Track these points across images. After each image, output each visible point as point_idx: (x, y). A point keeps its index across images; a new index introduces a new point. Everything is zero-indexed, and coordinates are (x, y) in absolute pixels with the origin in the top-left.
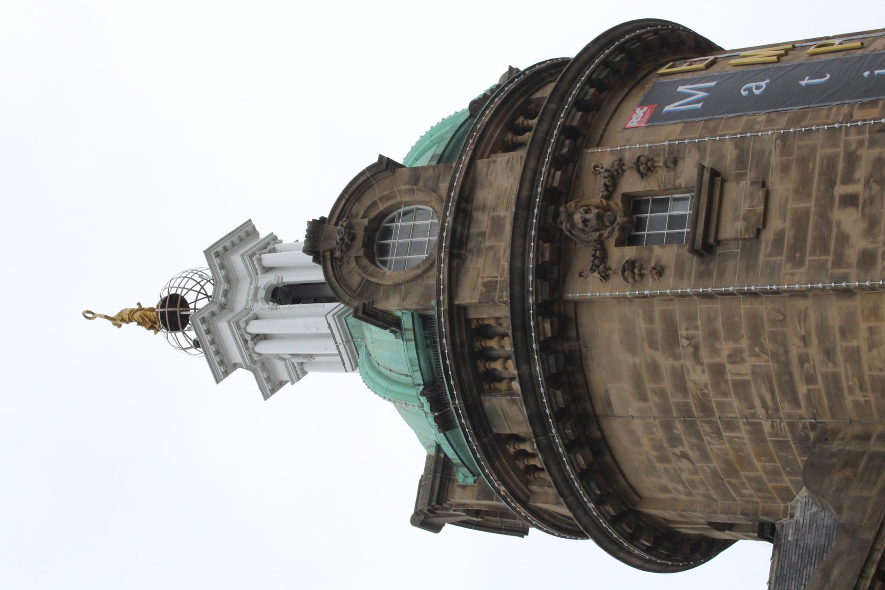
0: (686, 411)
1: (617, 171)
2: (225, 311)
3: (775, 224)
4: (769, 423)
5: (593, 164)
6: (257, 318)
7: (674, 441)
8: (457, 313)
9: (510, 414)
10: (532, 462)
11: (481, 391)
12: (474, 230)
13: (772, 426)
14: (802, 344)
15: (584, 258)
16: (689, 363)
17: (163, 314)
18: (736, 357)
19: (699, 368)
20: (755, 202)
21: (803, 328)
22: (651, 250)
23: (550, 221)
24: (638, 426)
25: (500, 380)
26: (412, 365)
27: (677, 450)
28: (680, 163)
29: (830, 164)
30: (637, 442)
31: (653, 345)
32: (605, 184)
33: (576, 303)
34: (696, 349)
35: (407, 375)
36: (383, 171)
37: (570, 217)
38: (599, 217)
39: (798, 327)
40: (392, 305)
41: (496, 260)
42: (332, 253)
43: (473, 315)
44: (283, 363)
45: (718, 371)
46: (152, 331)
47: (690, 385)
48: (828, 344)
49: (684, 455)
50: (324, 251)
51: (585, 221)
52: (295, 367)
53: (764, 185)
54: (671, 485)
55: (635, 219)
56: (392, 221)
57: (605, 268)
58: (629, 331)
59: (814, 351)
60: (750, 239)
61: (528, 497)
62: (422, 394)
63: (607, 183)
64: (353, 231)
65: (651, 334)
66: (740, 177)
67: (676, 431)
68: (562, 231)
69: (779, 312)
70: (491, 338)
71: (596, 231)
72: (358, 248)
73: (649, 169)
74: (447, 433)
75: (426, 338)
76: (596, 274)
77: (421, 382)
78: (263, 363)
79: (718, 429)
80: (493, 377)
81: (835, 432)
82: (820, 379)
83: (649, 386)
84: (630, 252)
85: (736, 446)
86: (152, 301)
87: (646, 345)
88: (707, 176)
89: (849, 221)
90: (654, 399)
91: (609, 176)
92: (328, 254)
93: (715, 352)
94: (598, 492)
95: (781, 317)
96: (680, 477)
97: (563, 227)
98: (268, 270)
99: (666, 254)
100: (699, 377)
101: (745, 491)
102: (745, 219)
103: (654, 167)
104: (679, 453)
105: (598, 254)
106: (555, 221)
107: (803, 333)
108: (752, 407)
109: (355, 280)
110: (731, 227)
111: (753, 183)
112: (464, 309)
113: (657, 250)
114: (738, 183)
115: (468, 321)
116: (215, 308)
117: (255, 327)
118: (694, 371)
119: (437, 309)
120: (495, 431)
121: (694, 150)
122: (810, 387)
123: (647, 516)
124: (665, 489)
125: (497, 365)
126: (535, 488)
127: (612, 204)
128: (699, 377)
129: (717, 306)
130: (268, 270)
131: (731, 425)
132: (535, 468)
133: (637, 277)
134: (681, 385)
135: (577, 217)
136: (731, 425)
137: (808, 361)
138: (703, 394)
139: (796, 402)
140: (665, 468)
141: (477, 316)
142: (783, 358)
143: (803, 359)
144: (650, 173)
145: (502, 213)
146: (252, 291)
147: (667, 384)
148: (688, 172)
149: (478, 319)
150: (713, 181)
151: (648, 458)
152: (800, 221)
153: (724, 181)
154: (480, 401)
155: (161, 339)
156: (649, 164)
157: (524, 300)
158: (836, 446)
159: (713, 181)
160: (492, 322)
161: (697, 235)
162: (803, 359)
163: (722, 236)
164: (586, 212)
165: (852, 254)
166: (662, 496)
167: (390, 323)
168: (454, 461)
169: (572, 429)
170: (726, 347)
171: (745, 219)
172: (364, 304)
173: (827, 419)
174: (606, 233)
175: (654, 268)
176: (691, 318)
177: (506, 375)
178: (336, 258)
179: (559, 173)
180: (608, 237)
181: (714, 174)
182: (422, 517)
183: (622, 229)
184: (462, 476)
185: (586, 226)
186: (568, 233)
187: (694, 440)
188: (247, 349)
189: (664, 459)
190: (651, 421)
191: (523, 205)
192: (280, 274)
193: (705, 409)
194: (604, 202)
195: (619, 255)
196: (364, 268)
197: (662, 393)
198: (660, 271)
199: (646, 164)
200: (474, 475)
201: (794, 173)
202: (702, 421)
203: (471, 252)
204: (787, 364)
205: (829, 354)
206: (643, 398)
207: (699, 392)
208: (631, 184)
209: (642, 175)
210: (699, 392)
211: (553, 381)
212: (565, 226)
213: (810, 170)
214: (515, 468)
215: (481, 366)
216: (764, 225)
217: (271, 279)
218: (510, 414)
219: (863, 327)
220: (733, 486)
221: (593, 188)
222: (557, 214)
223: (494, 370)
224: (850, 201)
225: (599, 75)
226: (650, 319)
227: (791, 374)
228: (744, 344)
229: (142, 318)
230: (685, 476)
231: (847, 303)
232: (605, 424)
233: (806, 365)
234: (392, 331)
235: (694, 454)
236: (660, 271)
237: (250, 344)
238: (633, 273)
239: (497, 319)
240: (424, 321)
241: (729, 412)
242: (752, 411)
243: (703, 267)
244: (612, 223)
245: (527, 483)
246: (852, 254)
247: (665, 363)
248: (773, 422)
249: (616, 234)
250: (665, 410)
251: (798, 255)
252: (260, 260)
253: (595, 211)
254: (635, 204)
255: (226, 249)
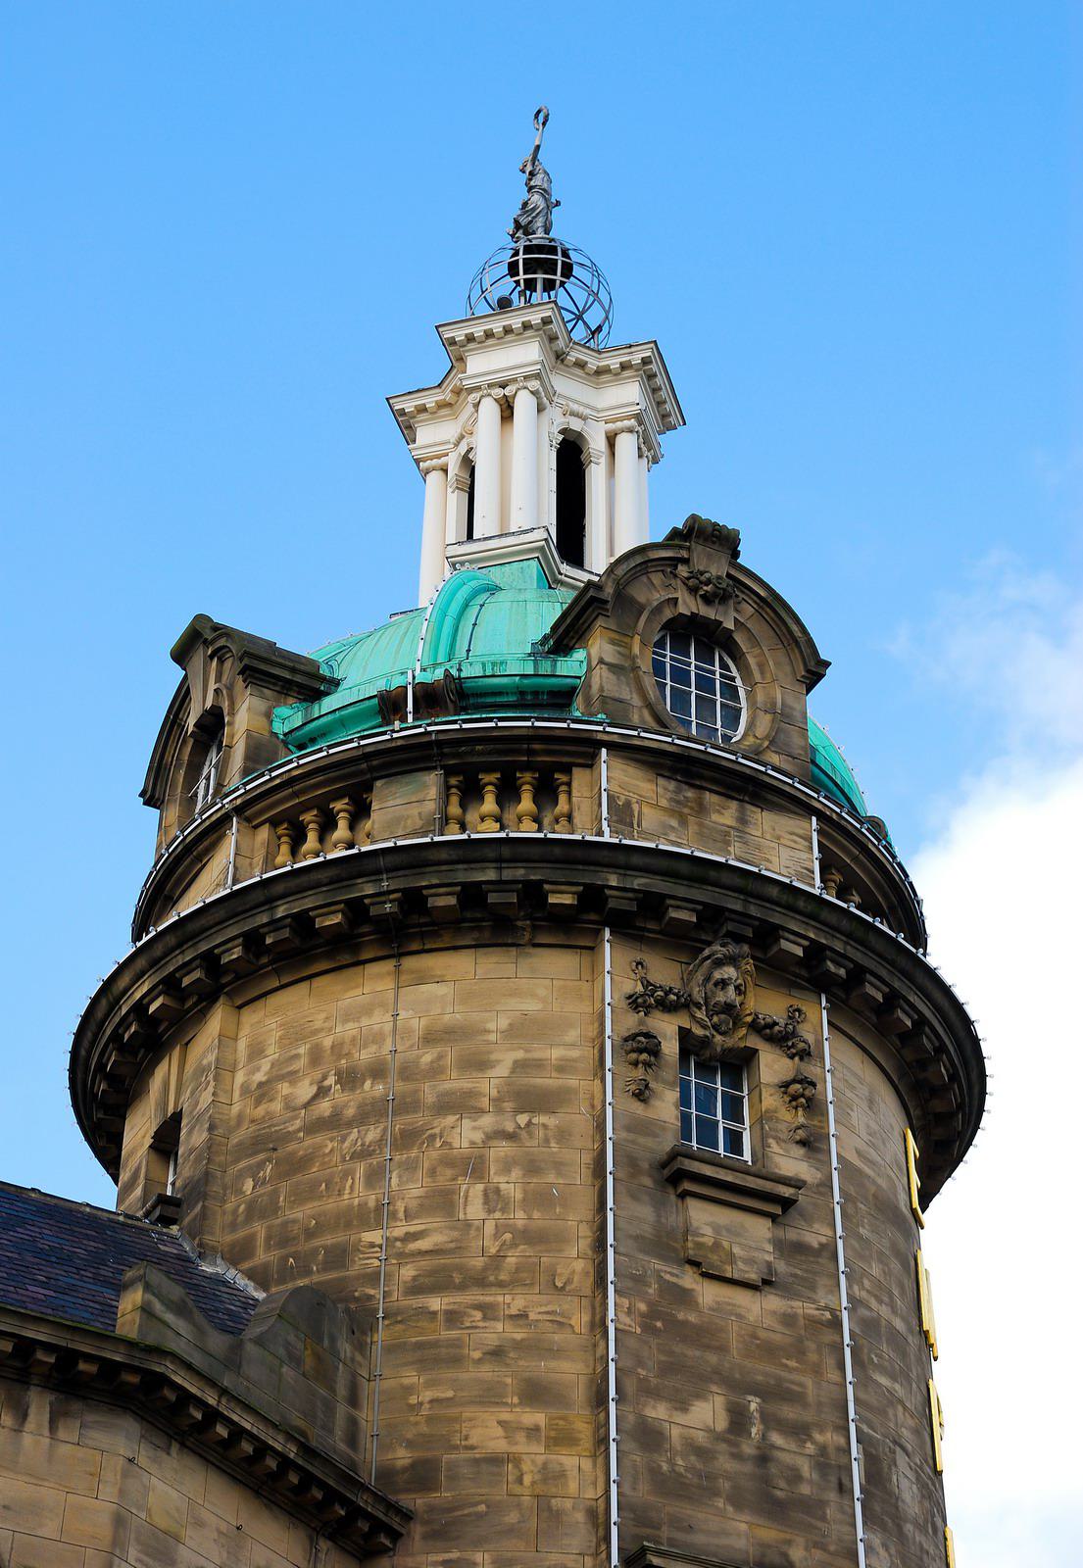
0: (406, 1105)
1: (793, 1046)
2: (553, 359)
3: (709, 1294)
4: (379, 1241)
5: (804, 1008)
6: (540, 409)
7: (350, 1079)
8: (584, 750)
9: (405, 813)
10: (312, 838)
11: (449, 772)
12: (710, 798)
13: (372, 1245)
14: (513, 1311)
15: (665, 972)
16: (487, 1121)
17: (553, 250)
18: (494, 1199)
19: (478, 1137)
20: (741, 1265)
21: (540, 1317)
22: (671, 1085)
23: (730, 926)
24: (380, 1021)
25: (463, 805)
26: (494, 664)
27: (331, 1080)
28: (800, 1151)
29: (795, 1398)
30: (348, 1017)
31: (519, 1066)
32: (775, 1024)
33: (593, 949)
34: (511, 1137)
35: (468, 651)
36: (805, 664)
37: (732, 960)
38: (728, 1008)
39: (543, 1309)
40: (599, 645)
41: (664, 832)
42: (686, 561)
43: (580, 777)
44: (453, 440)
45: (474, 1166)
46: (511, 227)
47: (451, 1119)
48: (511, 1355)
49: (322, 1092)
50: (689, 549)
51: (723, 984)
52: (438, 457)
53: (766, 1282)
54: (265, 1065)
55: (713, 1063)
56: (724, 666)
57: (650, 1006)
58: (529, 1030)
59: (497, 1332)
60: (685, 1249)
61: (248, 820)
62: (447, 673)
63: (777, 1028)
64: (717, 601)
65: (538, 1065)
66: (780, 1245)
67: (368, 1084)
68: (709, 944)
69: (569, 1281)
70: (499, 802)
71: (706, 998)
72: (688, 605)
73: (794, 1098)
74: (375, 701)
75: (536, 693)
76: (640, 988)
77: (463, 675)
78: (449, 405)
79: (370, 1154)
80: (471, 793)
81: (361, 1347)
82: (454, 1333)
83: (451, 1054)
84: (671, 1048)
85: (337, 1180)
86: (563, 231)
87: (520, 1055)
88: (786, 1192)
89: (708, 1413)
90: (427, 1058)
91: (787, 1032)
92: (684, 554)
93: (506, 1167)
94: (269, 941)
95: (559, 1284)
96: (281, 1078)
97: (717, 947)
98: (611, 441)
99: (666, 1107)
100: (466, 1134)
101: (249, 1185)
102: (717, 1245)
103: (796, 1108)
104: (326, 1083)
105: (673, 997)
106: (730, 935)
107: (532, 1316)
108: (408, 1216)
109: (640, 593)
110: (705, 1219)
111: (769, 1264)
112: (590, 762)
113: (672, 1096)
114: (769, 1241)
115: (567, 769)
116: (561, 343)
117: (524, 404)
118: (474, 1128)
119: (577, 720)
120: (378, 784)
121: (819, 1175)
122: (441, 1317)
123: (202, 1015)
124: (256, 1052)
125: (489, 804)
126: (264, 833)
127: (743, 1031)
128: (466, 1134)
129: (580, 1177)
130: (611, 441)
131: (375, 1176)
132: (298, 839)
133: (634, 1056)
134: (460, 1105)
135: (729, 972)
136: (375, 1176)
137: (485, 1318)
138: (433, 1137)
139: (416, 1288)
140: (297, 1056)
141: (575, 784)
142: (492, 1278)
143: (488, 1311)
144: (787, 1099)
145: (736, 848)
146: (581, 410)
147: (455, 1082)
148: (790, 1163)
149: (569, 784)
150: (776, 1202)
151: (315, 1032)
152: (705, 1335)
153: (774, 1218)
154: (434, 768)
155: (498, 243)
156: (803, 1100)
157: (613, 866)
158: (345, 1348)
159: (776, 1202)
160: (562, 805)
161: (697, 1163)
162: (488, 1311)
163: (691, 1202)
164: (737, 988)
165: (658, 1411)
166: (242, 1045)
167: (565, 637)
168: (316, 707)
169: (390, 913)
170: (511, 1185)
171: (717, 1245)
172: (606, 602)
173: (381, 1336)
174: (700, 1015)
175: (647, 1086)
176: (563, 1135)
177: (472, 817)
178: (676, 567)
179: (799, 952)
180: (693, 1017)
181: (787, 1204)
182: (209, 635)
183: (705, 1042)
184: (289, 717)
185: (716, 984)
186: (706, 952)
187: (350, 1112)
188: (490, 386)
189: (316, 1057)
190: (388, 1046)
191: (752, 884)
192: (603, 460)
193: (408, 1138)
194: (749, 1019)
195: (667, 1028)
196: (658, 609)
197: (435, 1071)
198: (642, 1094)
199: (803, 1096)
200: (285, 735)
201: (780, 1337)
202: (385, 1130)
203: (678, 791)
204: (480, 1281)
205: (496, 1354)
206: (430, 1038)
207: (437, 1131)
208: (772, 1066)
209: (786, 1085)
210: (437, 1131)
211: (472, 895)
212: (718, 949)
213: (784, 1361)
214: (305, 807)
215: (489, 778)
216: (706, 1275)
217: (596, 443)
218: (405, 813)
219: (537, 1417)
220: (261, 1165)
221: (770, 1005)
222: (738, 939)
223: (482, 799)
224: (738, 1421)
225: (927, 1037)
226: (563, 1067)
227: (462, 1287)
228: (519, 1218)
229: (534, 209)
230: (284, 1088)
231: (580, 1394)
232: (388, 966)
233: (478, 1315)
234: (546, 638)
235: (325, 1107)
236: (642, 1094)
237: (498, 392)
238: (640, 1051)
239: (569, 817)
240: (561, 698)
241: (400, 1177)
242: (401, 1215)
243: (645, 1166)
244: (715, 1027)
245: (274, 823)
246: (658, 1411)
247: (489, 1084)
248: (380, 1246)
249: (698, 1031)
250: (407, 1072)
251: (659, 1324)
252: (630, 430)
253: (738, 1000)
254: (737, 1065)
255: (651, 376)
